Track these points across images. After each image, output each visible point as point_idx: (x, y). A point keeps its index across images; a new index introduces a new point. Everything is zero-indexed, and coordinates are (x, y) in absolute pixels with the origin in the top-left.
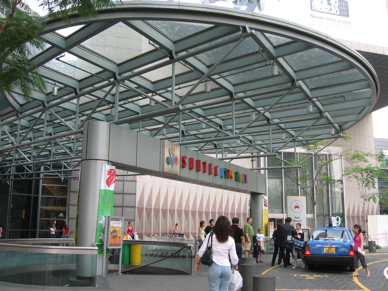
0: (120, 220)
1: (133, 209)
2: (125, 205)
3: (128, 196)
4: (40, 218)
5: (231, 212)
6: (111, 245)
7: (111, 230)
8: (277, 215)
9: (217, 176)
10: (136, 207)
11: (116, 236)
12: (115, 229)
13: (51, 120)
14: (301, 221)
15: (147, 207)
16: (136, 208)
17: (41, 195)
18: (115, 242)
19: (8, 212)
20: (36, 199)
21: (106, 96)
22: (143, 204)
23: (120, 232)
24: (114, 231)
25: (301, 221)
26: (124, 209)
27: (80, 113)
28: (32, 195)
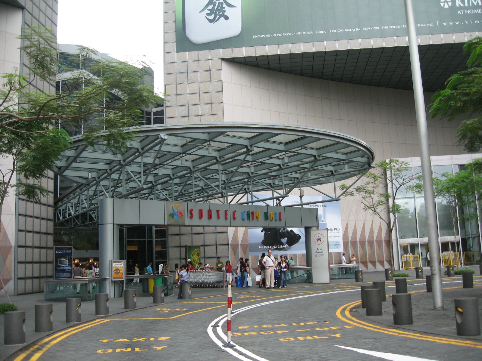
0: (122, 262)
1: (226, 247)
2: (218, 243)
3: (221, 234)
4: (156, 259)
5: (352, 241)
6: (114, 278)
7: (114, 269)
8: (410, 239)
9: (236, 220)
10: (230, 243)
11: (119, 273)
12: (118, 268)
13: (161, 162)
14: (322, 252)
15: (242, 243)
16: (230, 246)
17: (155, 238)
18: (118, 276)
19: (125, 256)
20: (151, 242)
21: (154, 161)
22: (238, 241)
23: (122, 270)
24: (117, 269)
25: (322, 252)
26: (218, 247)
27: (144, 172)
28: (146, 239)
